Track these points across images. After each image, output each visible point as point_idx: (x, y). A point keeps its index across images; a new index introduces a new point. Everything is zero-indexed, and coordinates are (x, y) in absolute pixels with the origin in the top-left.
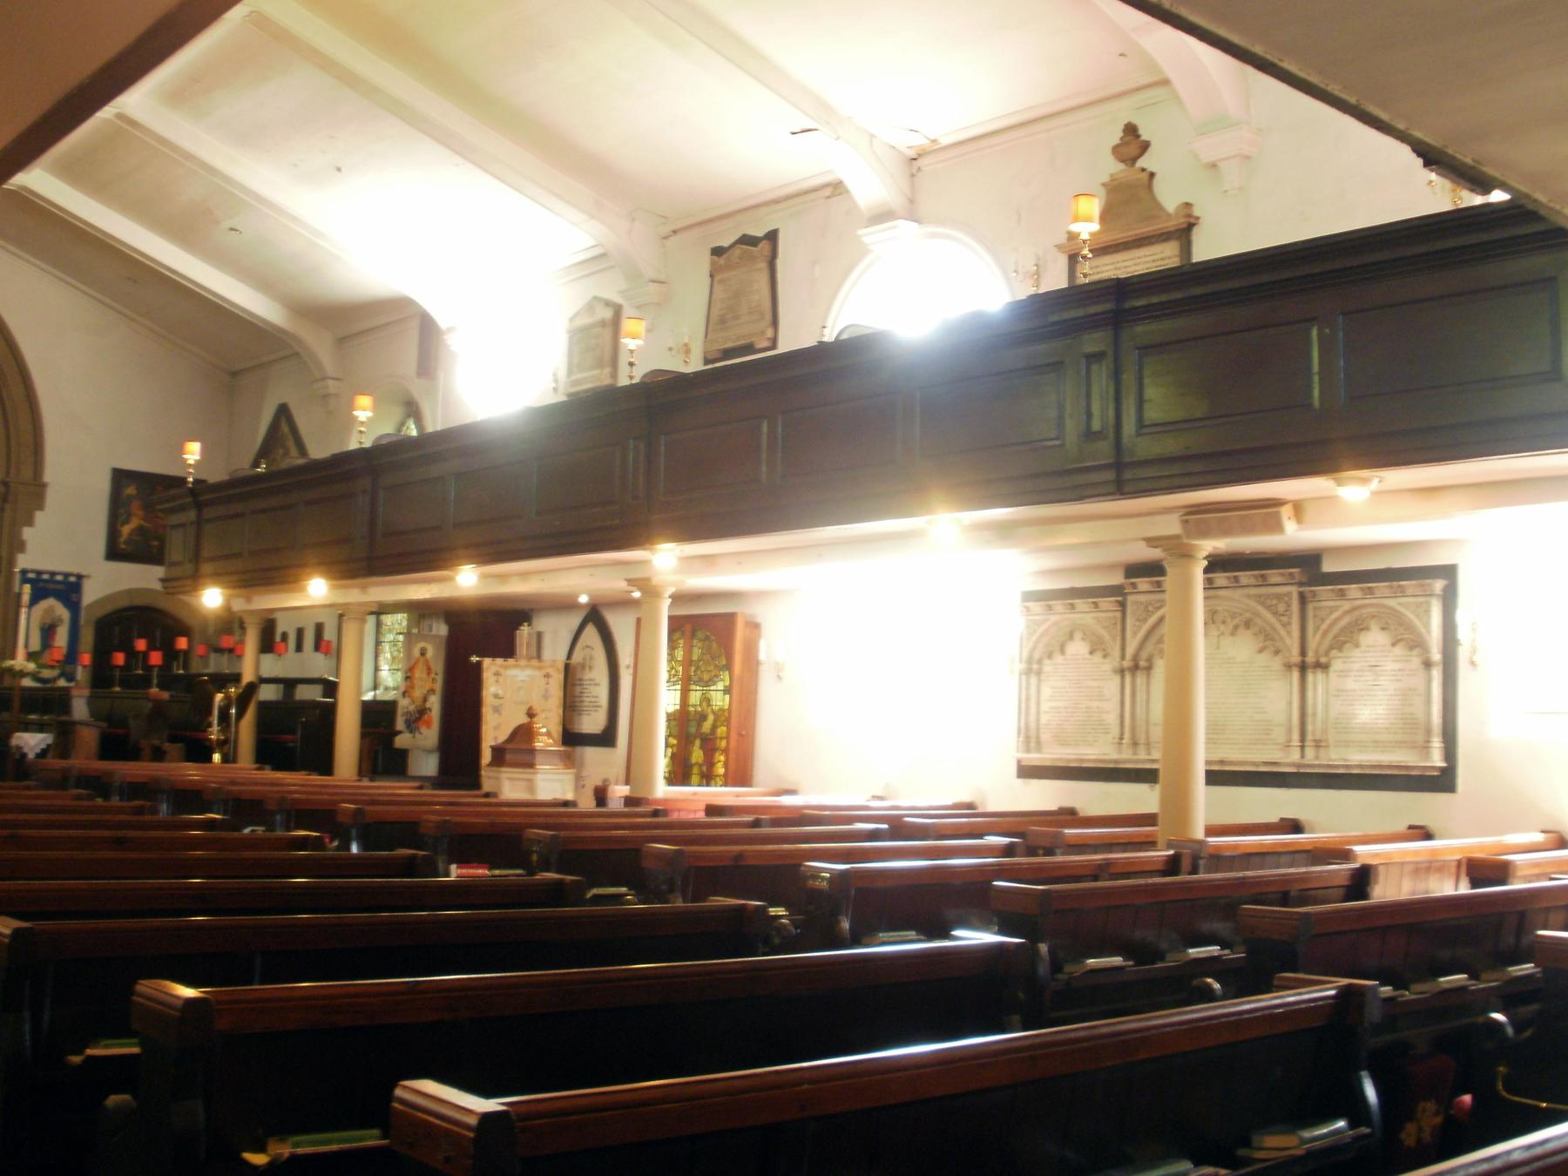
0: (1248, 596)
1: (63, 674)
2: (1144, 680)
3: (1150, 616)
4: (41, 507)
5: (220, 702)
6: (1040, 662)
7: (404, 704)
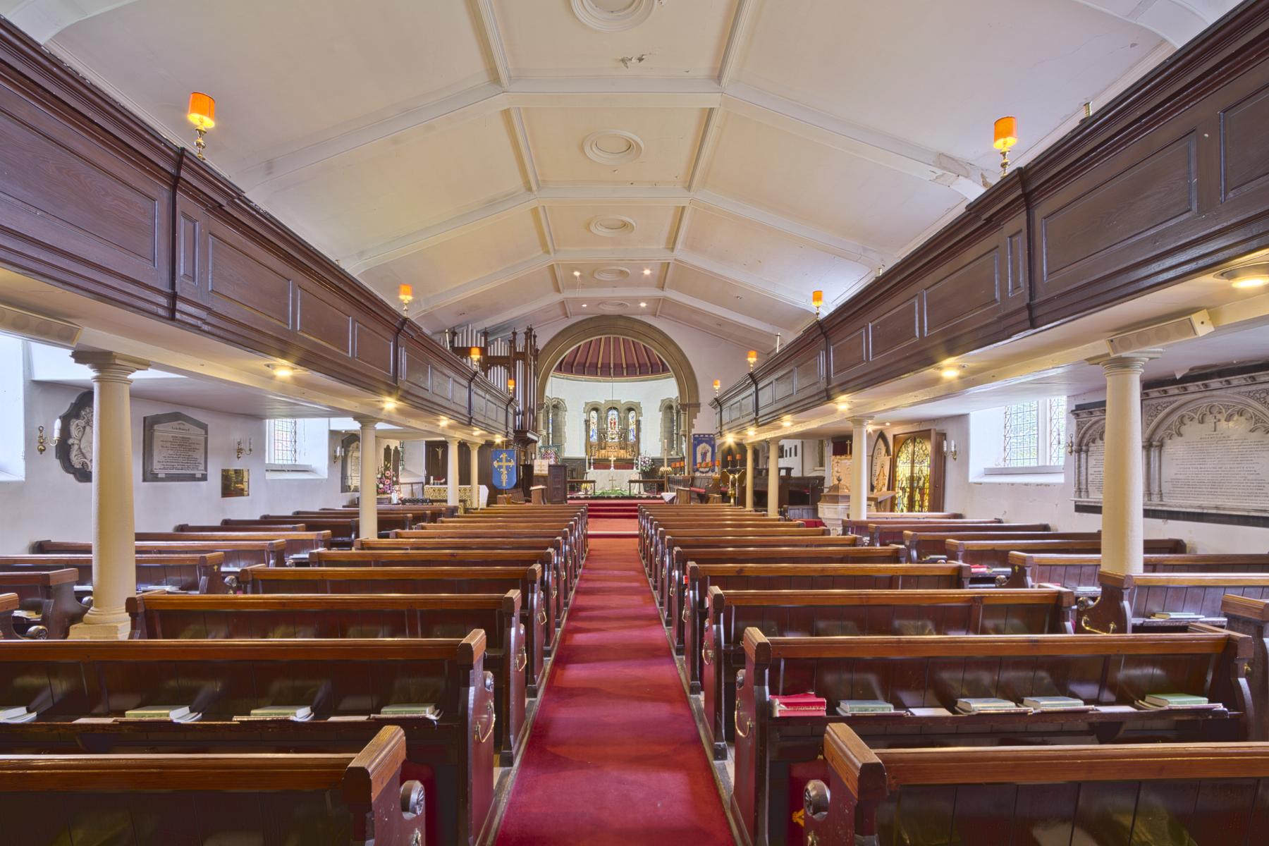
0: (1239, 393)
2: (1157, 454)
3: (1160, 413)
6: (1087, 445)
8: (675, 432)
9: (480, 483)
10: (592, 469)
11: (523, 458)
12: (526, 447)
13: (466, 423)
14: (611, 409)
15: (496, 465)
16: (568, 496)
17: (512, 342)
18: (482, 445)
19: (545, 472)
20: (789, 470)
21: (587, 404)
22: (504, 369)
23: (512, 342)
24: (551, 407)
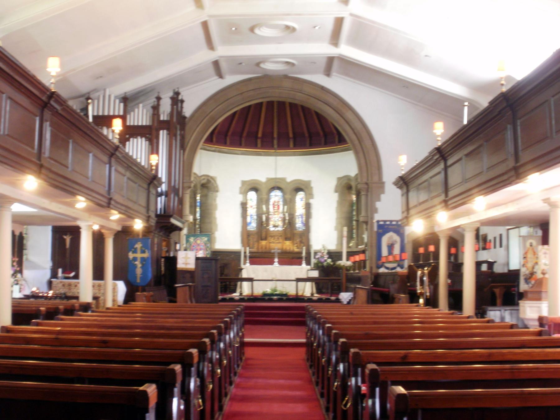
1: (399, 265)
4: (383, 192)
5: (420, 274)
7: (524, 271)
8: (355, 218)
9: (116, 277)
10: (248, 264)
11: (165, 249)
12: (168, 236)
13: (105, 204)
14: (273, 189)
15: (131, 255)
16: (220, 297)
17: (156, 108)
18: (119, 232)
19: (191, 265)
20: (491, 265)
21: (244, 183)
22: (146, 141)
23: (156, 108)
24: (199, 186)
